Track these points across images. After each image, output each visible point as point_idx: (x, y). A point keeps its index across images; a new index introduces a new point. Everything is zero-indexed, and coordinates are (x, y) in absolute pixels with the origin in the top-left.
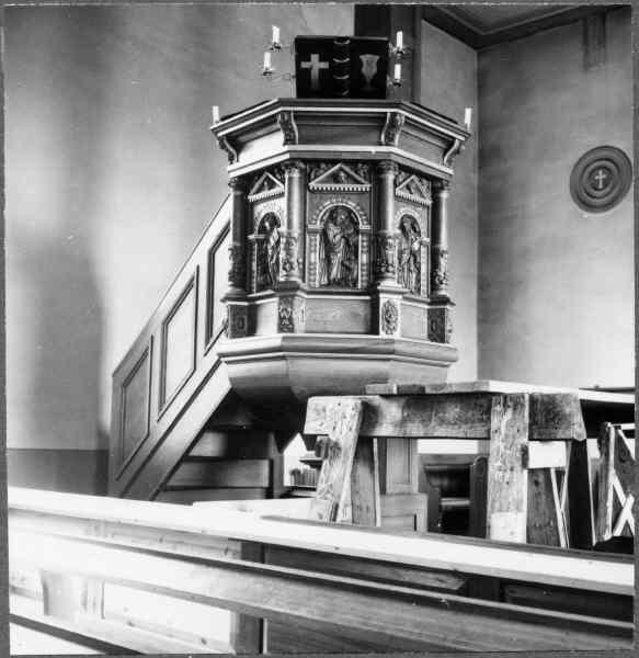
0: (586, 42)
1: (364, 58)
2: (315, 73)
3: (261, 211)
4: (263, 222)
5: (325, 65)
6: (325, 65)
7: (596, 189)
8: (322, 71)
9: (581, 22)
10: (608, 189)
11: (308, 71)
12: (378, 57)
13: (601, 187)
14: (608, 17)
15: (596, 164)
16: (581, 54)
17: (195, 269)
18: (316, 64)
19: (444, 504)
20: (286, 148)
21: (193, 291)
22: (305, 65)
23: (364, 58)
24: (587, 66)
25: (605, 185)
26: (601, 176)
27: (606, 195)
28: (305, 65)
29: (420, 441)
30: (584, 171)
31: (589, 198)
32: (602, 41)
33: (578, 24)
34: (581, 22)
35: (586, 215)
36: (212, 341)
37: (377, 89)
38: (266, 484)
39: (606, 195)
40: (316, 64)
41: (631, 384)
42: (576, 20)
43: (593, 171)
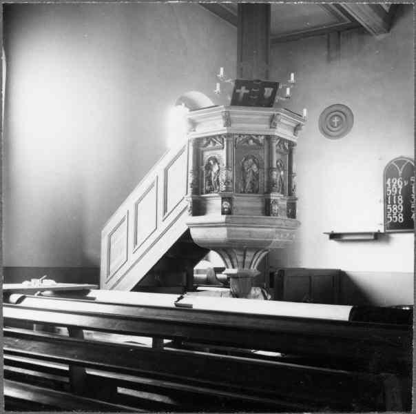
0: (329, 47)
1: (266, 89)
2: (242, 95)
3: (207, 155)
4: (209, 160)
5: (248, 91)
6: (248, 91)
7: (332, 126)
8: (245, 94)
9: (326, 36)
10: (339, 127)
11: (238, 94)
12: (272, 89)
13: (336, 125)
14: (342, 33)
15: (333, 114)
16: (326, 53)
17: (155, 178)
18: (243, 90)
19: (88, 372)
20: (225, 128)
21: (155, 188)
22: (238, 91)
23: (266, 89)
24: (329, 59)
25: (338, 125)
26: (336, 120)
27: (338, 130)
28: (238, 91)
29: (378, 225)
30: (327, 116)
31: (328, 131)
32: (338, 47)
33: (324, 36)
34: (326, 36)
35: (326, 139)
36: (167, 214)
37: (269, 103)
38: (185, 284)
39: (338, 130)
40: (243, 90)
41: (4, 308)
42: (323, 34)
43: (331, 118)
